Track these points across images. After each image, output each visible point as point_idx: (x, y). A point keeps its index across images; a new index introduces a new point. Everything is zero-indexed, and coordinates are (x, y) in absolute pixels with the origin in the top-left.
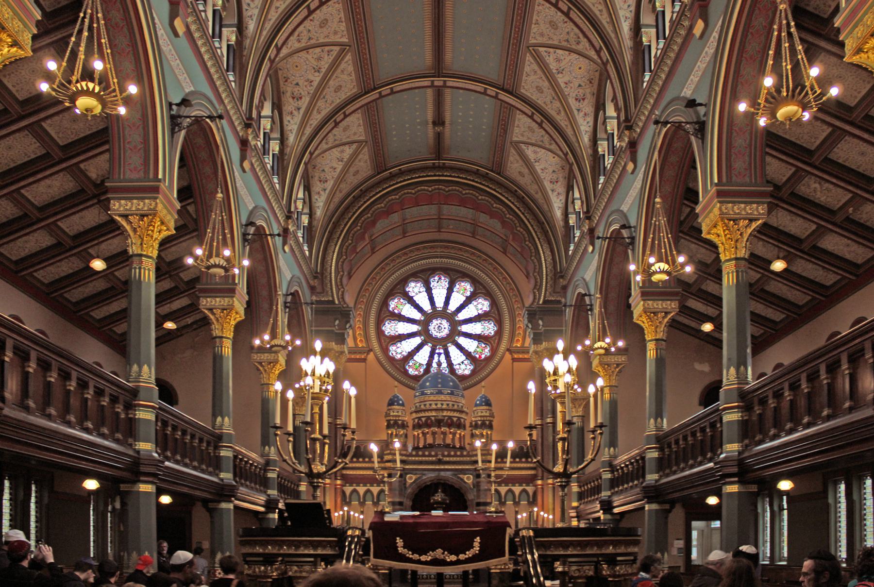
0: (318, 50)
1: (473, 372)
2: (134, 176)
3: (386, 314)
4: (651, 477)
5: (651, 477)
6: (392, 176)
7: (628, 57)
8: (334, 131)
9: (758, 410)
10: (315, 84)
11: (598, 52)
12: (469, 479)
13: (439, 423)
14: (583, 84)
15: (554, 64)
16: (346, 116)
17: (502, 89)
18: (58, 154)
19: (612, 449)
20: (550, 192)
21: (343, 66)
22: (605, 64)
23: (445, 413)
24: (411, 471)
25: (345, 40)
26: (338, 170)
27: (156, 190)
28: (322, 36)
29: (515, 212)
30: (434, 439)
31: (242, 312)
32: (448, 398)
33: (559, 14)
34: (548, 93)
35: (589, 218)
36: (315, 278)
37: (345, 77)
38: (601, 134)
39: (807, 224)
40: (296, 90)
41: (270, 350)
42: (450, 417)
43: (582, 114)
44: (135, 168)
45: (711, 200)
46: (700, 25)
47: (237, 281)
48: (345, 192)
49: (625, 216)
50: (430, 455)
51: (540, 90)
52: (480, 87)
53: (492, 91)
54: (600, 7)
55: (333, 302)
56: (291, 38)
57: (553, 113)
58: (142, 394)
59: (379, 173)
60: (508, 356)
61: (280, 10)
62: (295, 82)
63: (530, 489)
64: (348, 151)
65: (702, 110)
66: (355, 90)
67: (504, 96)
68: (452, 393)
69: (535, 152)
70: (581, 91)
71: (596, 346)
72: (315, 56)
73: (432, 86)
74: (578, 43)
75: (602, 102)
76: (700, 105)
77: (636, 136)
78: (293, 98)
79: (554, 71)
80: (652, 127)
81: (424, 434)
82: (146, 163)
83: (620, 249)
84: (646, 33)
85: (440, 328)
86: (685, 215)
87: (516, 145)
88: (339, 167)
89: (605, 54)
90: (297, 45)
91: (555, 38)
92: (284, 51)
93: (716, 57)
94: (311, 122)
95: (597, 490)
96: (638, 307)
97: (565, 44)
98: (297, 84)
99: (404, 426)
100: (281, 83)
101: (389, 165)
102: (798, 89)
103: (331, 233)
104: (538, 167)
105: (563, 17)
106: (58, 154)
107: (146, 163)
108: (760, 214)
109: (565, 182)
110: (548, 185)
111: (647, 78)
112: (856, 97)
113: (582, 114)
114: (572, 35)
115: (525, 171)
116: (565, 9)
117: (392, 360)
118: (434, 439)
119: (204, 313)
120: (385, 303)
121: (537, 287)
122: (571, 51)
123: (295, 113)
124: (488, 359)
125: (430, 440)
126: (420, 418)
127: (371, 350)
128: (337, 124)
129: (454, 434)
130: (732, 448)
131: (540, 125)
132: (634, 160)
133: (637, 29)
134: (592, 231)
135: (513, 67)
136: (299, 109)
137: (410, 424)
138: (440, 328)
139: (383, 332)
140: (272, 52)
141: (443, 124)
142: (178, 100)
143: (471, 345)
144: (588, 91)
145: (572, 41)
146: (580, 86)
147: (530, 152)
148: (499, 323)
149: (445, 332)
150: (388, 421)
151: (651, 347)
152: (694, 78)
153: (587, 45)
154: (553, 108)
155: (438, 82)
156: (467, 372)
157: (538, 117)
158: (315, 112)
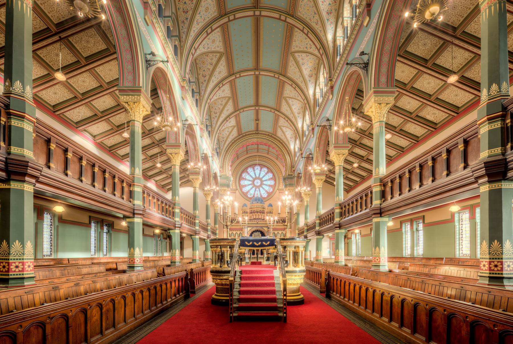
1: (268, 196)
2: (173, 142)
4: (317, 228)
5: (317, 228)
8: (219, 91)
10: (211, 70)
11: (304, 100)
12: (266, 229)
16: (223, 85)
18: (106, 86)
19: (494, 87)
21: (229, 103)
22: (306, 104)
25: (230, 96)
27: (140, 91)
33: (304, 35)
34: (289, 111)
37: (222, 67)
39: (365, 152)
40: (185, 6)
41: (209, 191)
43: (329, 22)
49: (311, 151)
52: (269, 110)
53: (273, 111)
56: (200, 46)
58: (176, 205)
59: (236, 111)
60: (278, 191)
61: (195, 32)
62: (184, 2)
63: (284, 232)
64: (230, 129)
65: (331, 122)
66: (226, 74)
67: (276, 112)
73: (255, 74)
76: (366, 54)
78: (184, 12)
82: (134, 79)
83: (325, 130)
86: (401, 43)
87: (280, 127)
88: (228, 134)
94: (210, 86)
95: (303, 232)
96: (314, 179)
97: (305, 49)
98: (185, 3)
99: (247, 213)
101: (243, 132)
102: (351, 125)
107: (134, 79)
111: (338, 59)
112: (470, 9)
114: (308, 45)
115: (283, 135)
116: (306, 32)
117: (243, 193)
120: (241, 175)
121: (286, 170)
124: (272, 192)
125: (255, 217)
128: (227, 121)
130: (376, 202)
134: (302, 154)
135: (285, 65)
136: (187, 19)
138: (258, 183)
140: (209, 101)
142: (184, 119)
144: (333, 8)
145: (296, 96)
147: (284, 129)
148: (275, 180)
149: (259, 184)
151: (317, 190)
152: (364, 43)
154: (291, 116)
155: (257, 108)
156: (266, 196)
157: (286, 119)
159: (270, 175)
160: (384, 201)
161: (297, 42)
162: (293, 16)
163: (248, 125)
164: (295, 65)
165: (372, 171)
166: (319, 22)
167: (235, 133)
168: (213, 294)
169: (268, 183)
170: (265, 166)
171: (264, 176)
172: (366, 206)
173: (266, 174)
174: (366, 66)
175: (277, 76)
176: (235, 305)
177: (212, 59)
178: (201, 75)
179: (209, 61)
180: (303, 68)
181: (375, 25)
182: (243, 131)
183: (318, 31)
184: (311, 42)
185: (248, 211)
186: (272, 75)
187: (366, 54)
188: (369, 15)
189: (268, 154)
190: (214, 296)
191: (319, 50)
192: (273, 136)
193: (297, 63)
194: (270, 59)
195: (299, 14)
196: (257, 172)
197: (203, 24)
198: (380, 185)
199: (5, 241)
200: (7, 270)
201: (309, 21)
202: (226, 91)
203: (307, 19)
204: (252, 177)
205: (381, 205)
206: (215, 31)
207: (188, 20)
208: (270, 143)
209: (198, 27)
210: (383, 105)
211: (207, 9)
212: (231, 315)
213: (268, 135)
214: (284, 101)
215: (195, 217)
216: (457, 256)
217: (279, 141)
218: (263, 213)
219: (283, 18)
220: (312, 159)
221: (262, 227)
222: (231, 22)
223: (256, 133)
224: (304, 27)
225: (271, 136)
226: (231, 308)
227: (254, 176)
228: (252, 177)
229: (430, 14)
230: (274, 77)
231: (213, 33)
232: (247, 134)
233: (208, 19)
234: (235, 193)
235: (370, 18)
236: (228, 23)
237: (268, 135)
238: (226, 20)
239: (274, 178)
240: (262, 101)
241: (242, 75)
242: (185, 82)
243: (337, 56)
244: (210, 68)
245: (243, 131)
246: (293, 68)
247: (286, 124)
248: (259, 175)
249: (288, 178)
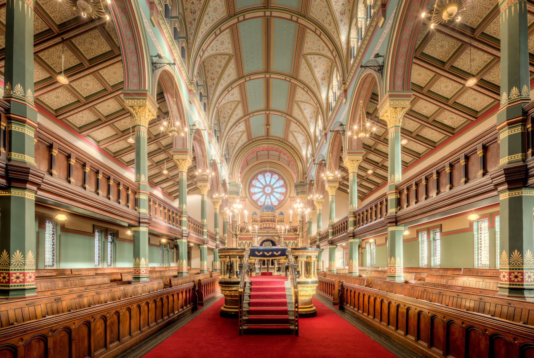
1: (279, 204)
2: (180, 148)
4: (330, 237)
5: (330, 237)
6: (253, 142)
9: (358, 217)
10: (219, 73)
11: (316, 104)
12: (277, 238)
16: (232, 89)
17: (292, 77)
18: (110, 89)
19: (515, 90)
20: (339, 21)
21: (238, 107)
22: (318, 108)
25: (239, 99)
27: (145, 95)
28: (222, 49)
31: (191, 162)
33: (316, 36)
34: (301, 116)
37: (231, 70)
40: (192, 7)
41: (217, 199)
43: (343, 23)
44: (135, 84)
46: (344, 100)
47: (147, 89)
49: (323, 157)
52: (280, 114)
53: (284, 115)
56: (209, 48)
58: (183, 213)
61: (203, 33)
62: (191, 2)
64: (240, 134)
65: (344, 127)
67: (287, 117)
69: (304, 106)
73: (265, 77)
76: (381, 56)
78: (191, 12)
80: (360, 69)
83: (339, 135)
87: (291, 132)
88: (237, 139)
89: (318, 106)
91: (314, 49)
94: (218, 89)
96: (327, 186)
97: (318, 51)
98: (193, 3)
99: (257, 221)
101: (253, 138)
102: (365, 130)
106: (56, 30)
107: (140, 82)
111: (352, 62)
114: (321, 46)
115: (294, 140)
116: (319, 34)
117: (253, 200)
119: (128, 109)
120: (251, 182)
121: (298, 177)
124: (283, 200)
125: (265, 226)
128: (236, 126)
130: (392, 211)
131: (299, 126)
134: (314, 160)
135: (296, 67)
136: (195, 20)
138: (268, 190)
140: (217, 105)
144: (347, 8)
145: (309, 100)
147: (296, 134)
148: (286, 188)
149: (270, 191)
151: (330, 197)
152: (379, 45)
154: (303, 121)
155: (268, 112)
156: (276, 204)
157: (298, 124)
158: (203, 23)
159: (281, 182)
160: (399, 210)
162: (305, 17)
163: (258, 130)
164: (307, 67)
165: (387, 178)
166: (332, 23)
167: (244, 139)
168: (222, 306)
169: (279, 190)
170: (276, 173)
171: (275, 183)
172: (381, 214)
173: (277, 181)
174: (381, 69)
175: (289, 80)
176: (244, 318)
180: (316, 71)
181: (390, 26)
182: (253, 137)
183: (332, 32)
184: (323, 44)
185: (259, 219)
187: (381, 56)
188: (384, 15)
189: (279, 160)
190: (222, 308)
191: (332, 52)
192: (284, 141)
193: (309, 65)
194: (281, 62)
195: (311, 14)
196: (268, 179)
197: (211, 25)
198: (396, 192)
199: (5, 251)
200: (7, 280)
201: (322, 22)
202: (235, 94)
203: (320, 20)
204: (262, 184)
205: (396, 213)
206: (224, 33)
207: (196, 21)
208: (281, 149)
210: (398, 109)
211: (215, 10)
212: (241, 328)
214: (295, 105)
215: (203, 226)
216: (476, 267)
217: (291, 147)
218: (274, 222)
219: (295, 18)
221: (272, 236)
222: (241, 23)
223: (266, 139)
224: (316, 29)
225: (282, 142)
226: (241, 321)
227: (264, 184)
228: (262, 184)
229: (447, 15)
230: (285, 80)
231: (222, 34)
232: (257, 139)
233: (216, 20)
234: (245, 200)
235: (385, 19)
236: (238, 24)
237: (279, 141)
238: (235, 20)
239: (285, 185)
240: (273, 106)
241: (252, 78)
242: (192, 86)
244: (218, 70)
245: (253, 137)
247: (298, 129)
248: (270, 182)
249: (300, 185)
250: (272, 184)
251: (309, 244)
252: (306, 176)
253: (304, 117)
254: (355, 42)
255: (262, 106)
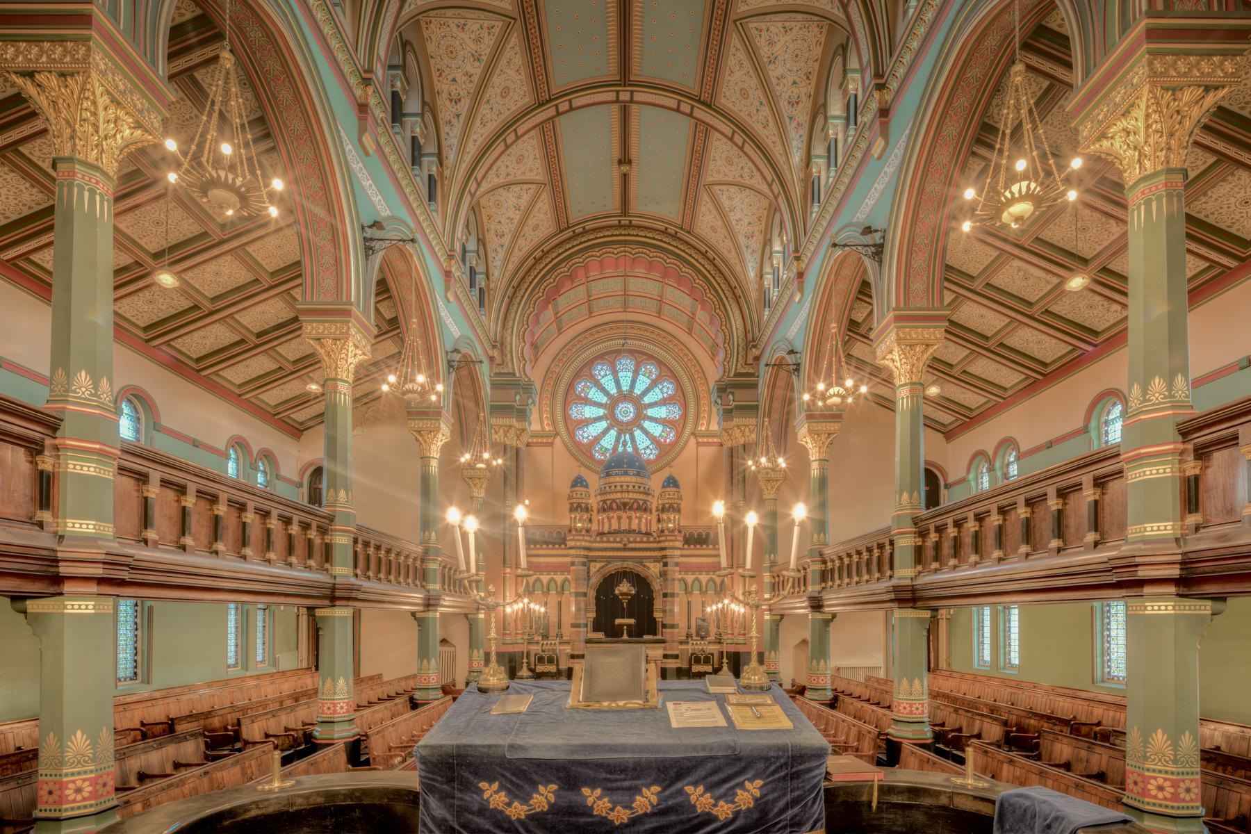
0: (517, 188)
1: (659, 457)
3: (571, 397)
6: (575, 236)
7: (797, 190)
9: (933, 537)
10: (476, 79)
13: (624, 506)
14: (798, 81)
15: (766, 49)
21: (539, 205)
23: (631, 495)
24: (595, 559)
25: (540, 178)
26: (516, 221)
28: (519, 172)
29: (705, 277)
30: (619, 524)
32: (634, 479)
34: (722, 232)
35: (798, 259)
36: (494, 347)
37: (511, 73)
38: (767, 269)
40: (453, 88)
42: (636, 500)
43: (794, 124)
45: (886, 327)
46: (880, 143)
48: (525, 250)
50: (614, 542)
51: (714, 229)
54: (774, 139)
55: (514, 375)
57: (757, 128)
59: (561, 231)
60: (693, 441)
62: (450, 77)
66: (526, 100)
68: (638, 474)
70: (796, 91)
71: (831, 391)
72: (473, 36)
74: (752, 177)
75: (821, 101)
76: (876, 231)
77: (888, 97)
78: (451, 100)
79: (765, 60)
81: (609, 519)
84: (853, 80)
85: (626, 412)
88: (517, 217)
89: (776, 188)
90: (497, 181)
92: (485, 186)
93: (900, 172)
94: (474, 137)
98: (454, 80)
100: (435, 79)
103: (511, 299)
104: (733, 217)
105: (739, 151)
108: (936, 339)
109: (761, 237)
110: (742, 241)
113: (794, 124)
115: (719, 224)
117: (578, 445)
118: (619, 524)
120: (571, 386)
122: (743, 187)
123: (454, 121)
124: (673, 444)
125: (615, 526)
126: (604, 501)
127: (557, 434)
129: (640, 519)
132: (885, 134)
133: (761, 277)
136: (458, 116)
137: (595, 507)
139: (570, 416)
141: (630, 162)
143: (656, 430)
146: (794, 83)
150: (572, 504)
152: (870, 202)
153: (760, 179)
158: (478, 122)
159: (668, 388)
161: (719, 163)
162: (709, 106)
164: (714, 212)
166: (771, 124)
169: (661, 412)
170: (651, 357)
177: (478, 40)
178: (445, 95)
179: (472, 46)
181: (897, 162)
182: (575, 217)
183: (769, 141)
184: (750, 164)
185: (594, 502)
186: (673, 104)
188: (885, 134)
189: (659, 314)
191: (770, 186)
192: (681, 234)
195: (723, 101)
197: (495, 124)
199: (1187, 733)
201: (747, 119)
202: (526, 157)
203: (742, 114)
204: (606, 393)
206: (525, 138)
207: (462, 119)
209: (483, 130)
211: (505, 92)
213: (665, 232)
217: (704, 255)
218: (645, 510)
219: (685, 108)
220: (797, 370)
221: (641, 560)
222: (561, 117)
223: (620, 226)
225: (675, 236)
228: (606, 393)
231: (520, 141)
232: (589, 226)
233: (507, 113)
234: (551, 444)
235: (887, 143)
236: (556, 119)
237: (665, 232)
238: (552, 112)
239: (680, 398)
240: (641, 67)
241: (576, 103)
243: (813, 201)
245: (575, 217)
246: (738, 74)
250: (637, 391)
251: (767, 587)
252: (755, 352)
253: (731, 234)
254: (823, 168)
255: (608, 67)
